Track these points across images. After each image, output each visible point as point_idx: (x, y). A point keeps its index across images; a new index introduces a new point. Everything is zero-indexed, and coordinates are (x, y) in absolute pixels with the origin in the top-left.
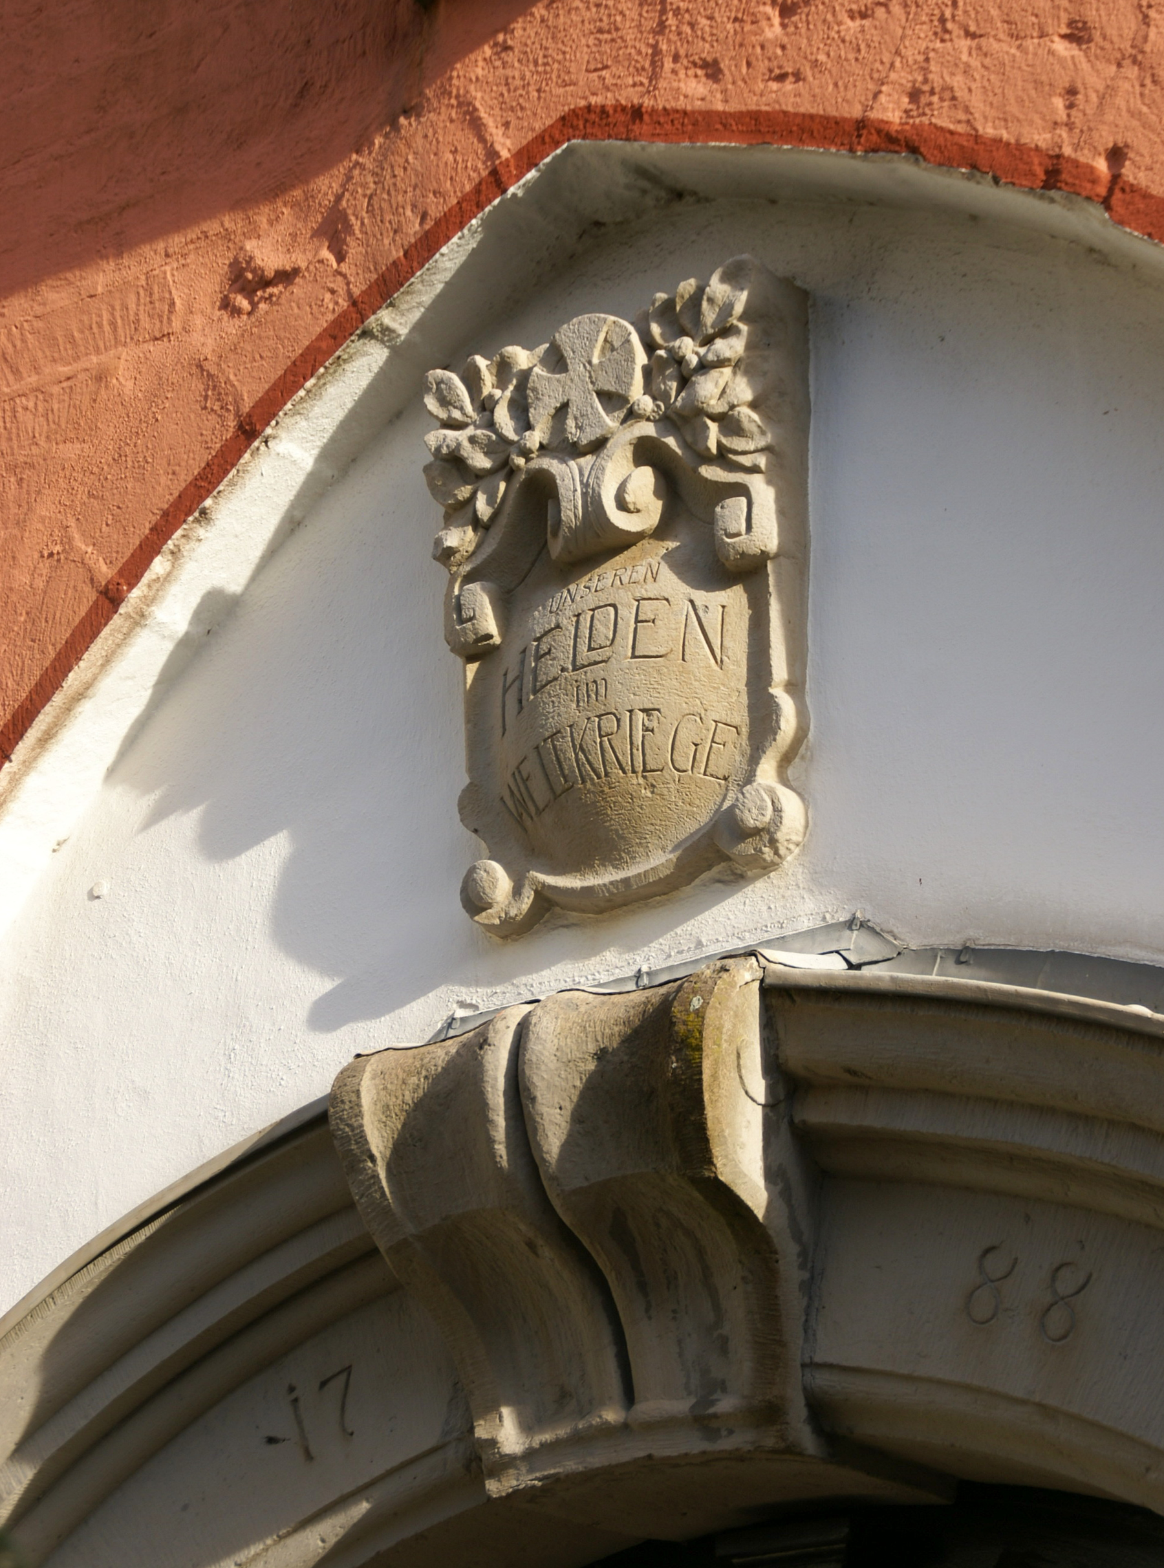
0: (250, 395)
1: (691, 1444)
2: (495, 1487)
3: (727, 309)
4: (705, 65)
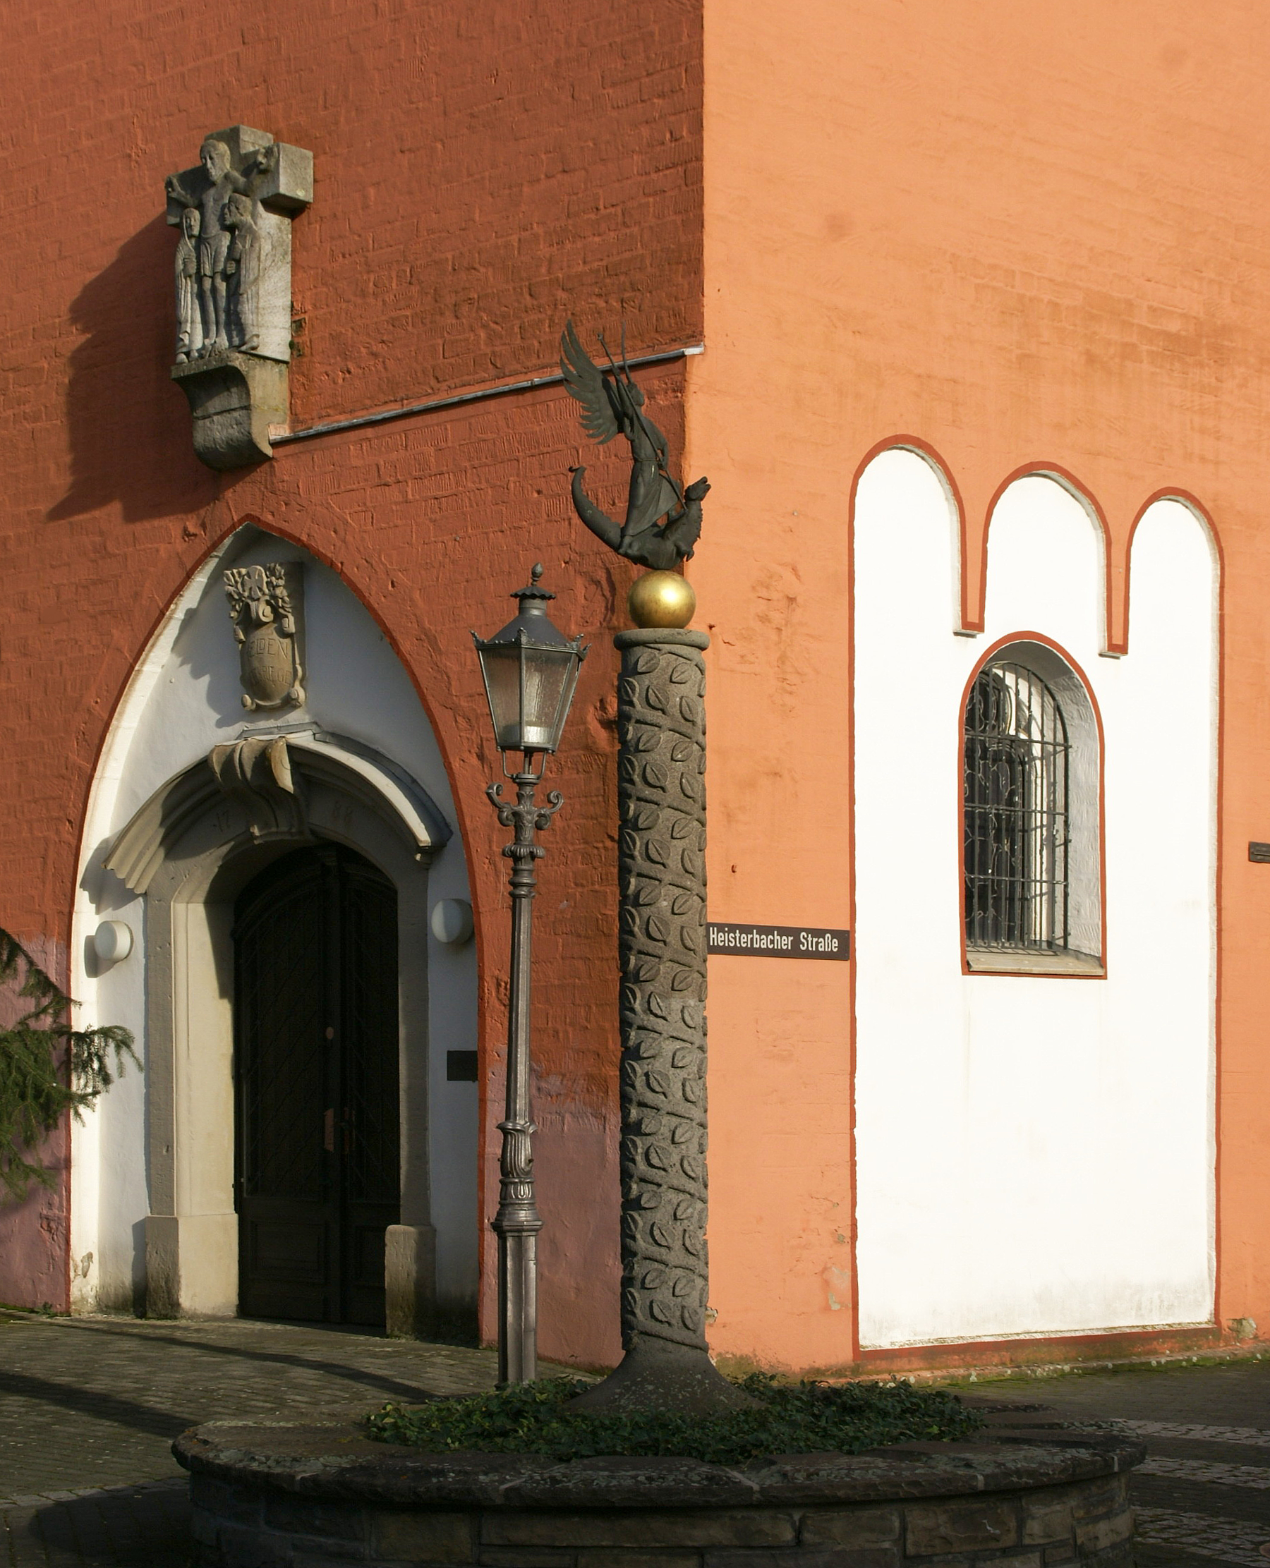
0: (189, 567)
1: (287, 837)
2: (256, 842)
3: (280, 573)
4: (474, 117)
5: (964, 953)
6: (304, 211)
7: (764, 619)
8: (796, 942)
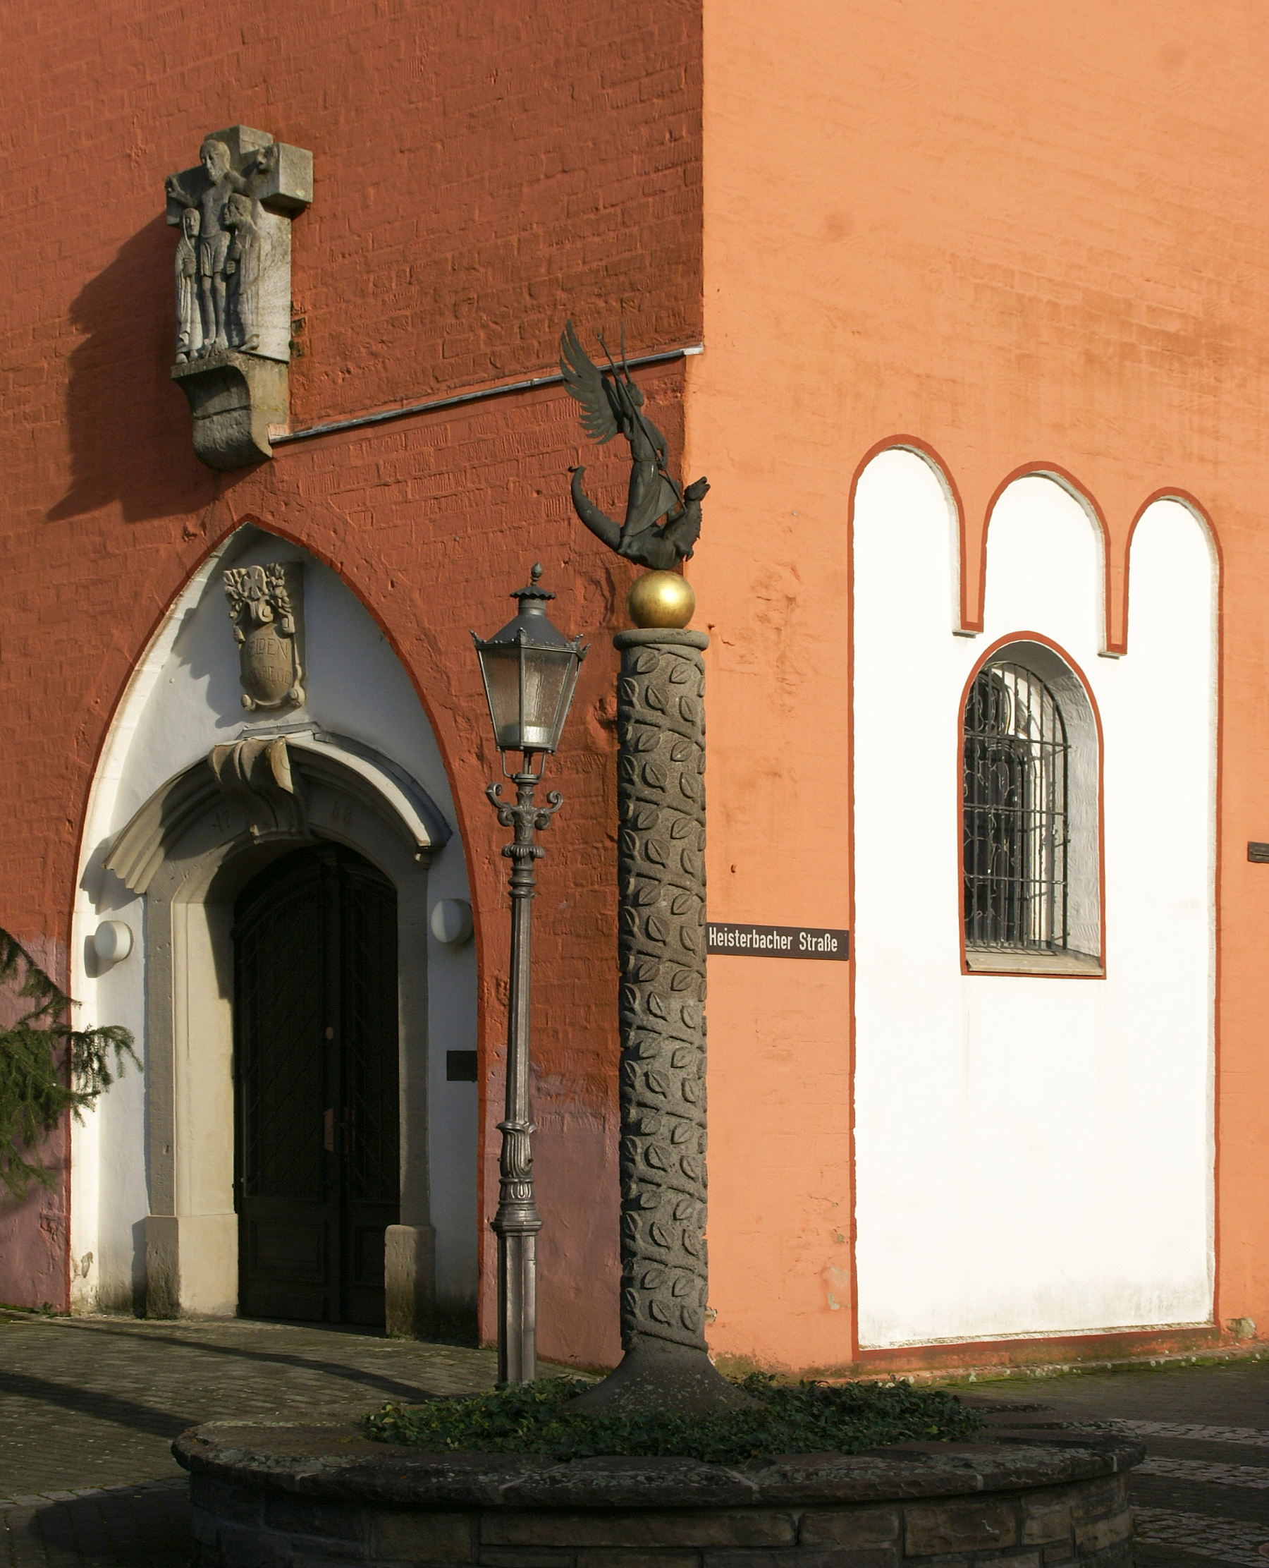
0: (189, 567)
1: (287, 837)
2: (256, 842)
3: (280, 573)
5: (963, 953)
6: (304, 211)
7: (764, 619)
8: (796, 942)
